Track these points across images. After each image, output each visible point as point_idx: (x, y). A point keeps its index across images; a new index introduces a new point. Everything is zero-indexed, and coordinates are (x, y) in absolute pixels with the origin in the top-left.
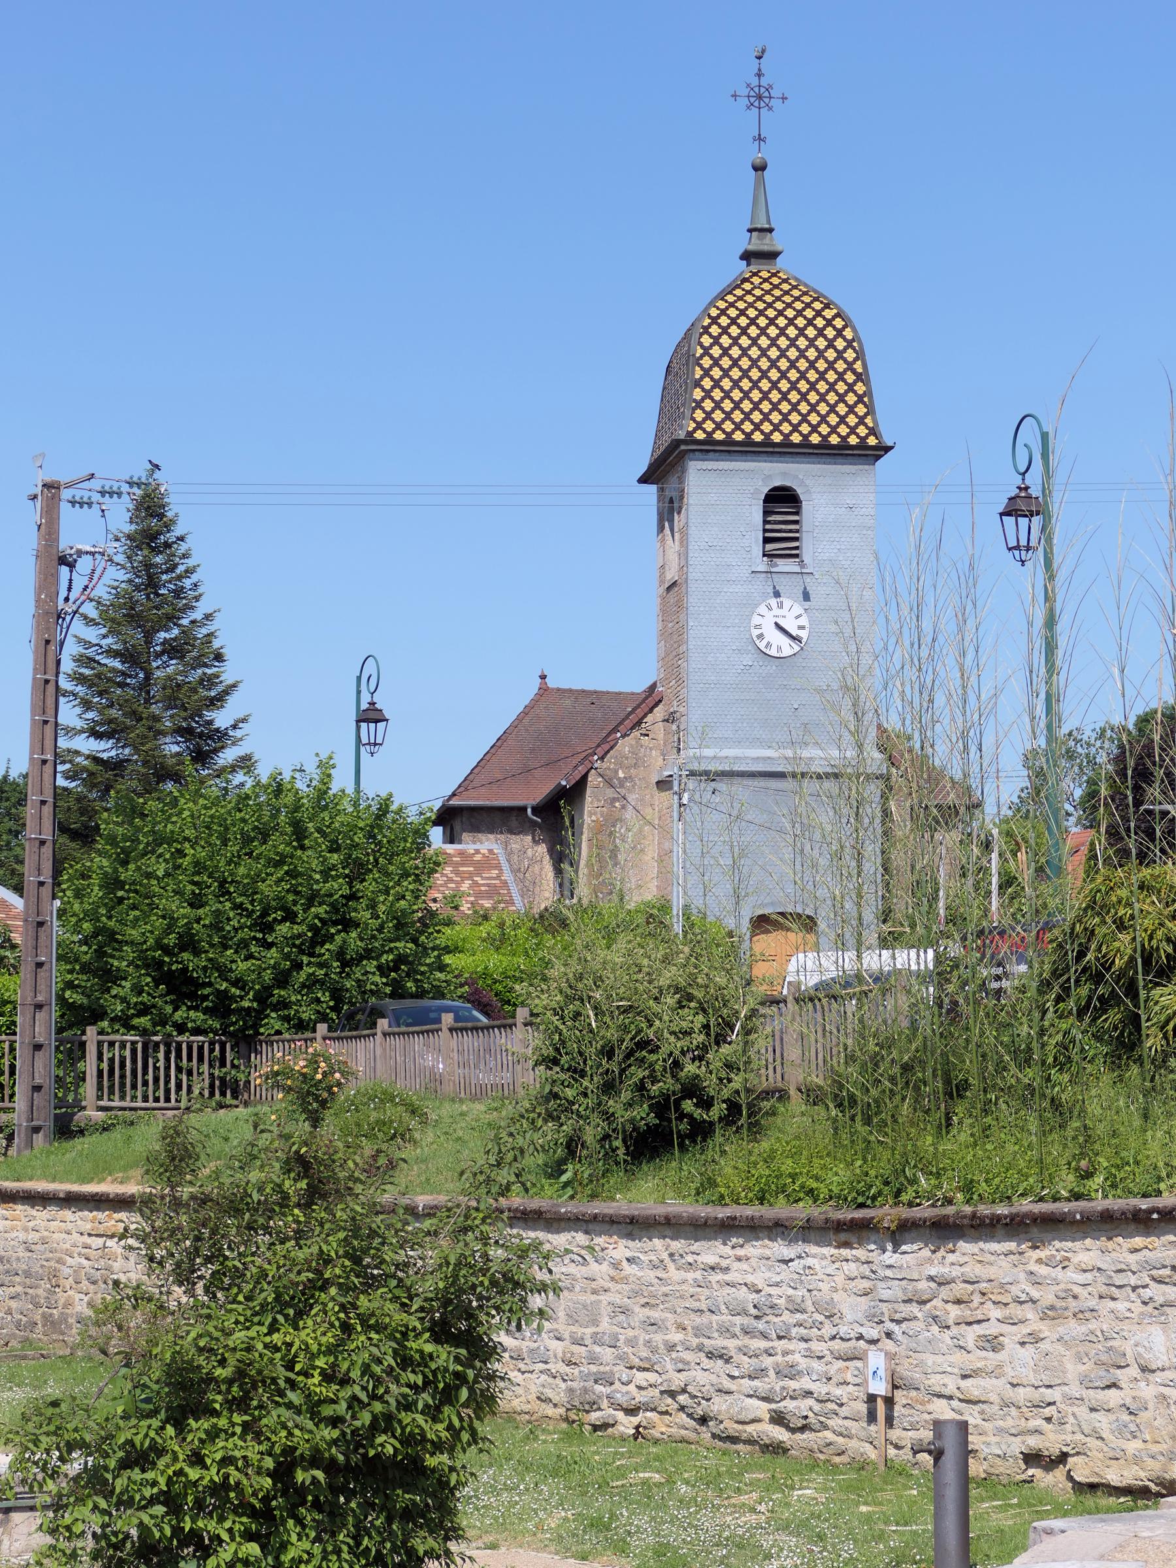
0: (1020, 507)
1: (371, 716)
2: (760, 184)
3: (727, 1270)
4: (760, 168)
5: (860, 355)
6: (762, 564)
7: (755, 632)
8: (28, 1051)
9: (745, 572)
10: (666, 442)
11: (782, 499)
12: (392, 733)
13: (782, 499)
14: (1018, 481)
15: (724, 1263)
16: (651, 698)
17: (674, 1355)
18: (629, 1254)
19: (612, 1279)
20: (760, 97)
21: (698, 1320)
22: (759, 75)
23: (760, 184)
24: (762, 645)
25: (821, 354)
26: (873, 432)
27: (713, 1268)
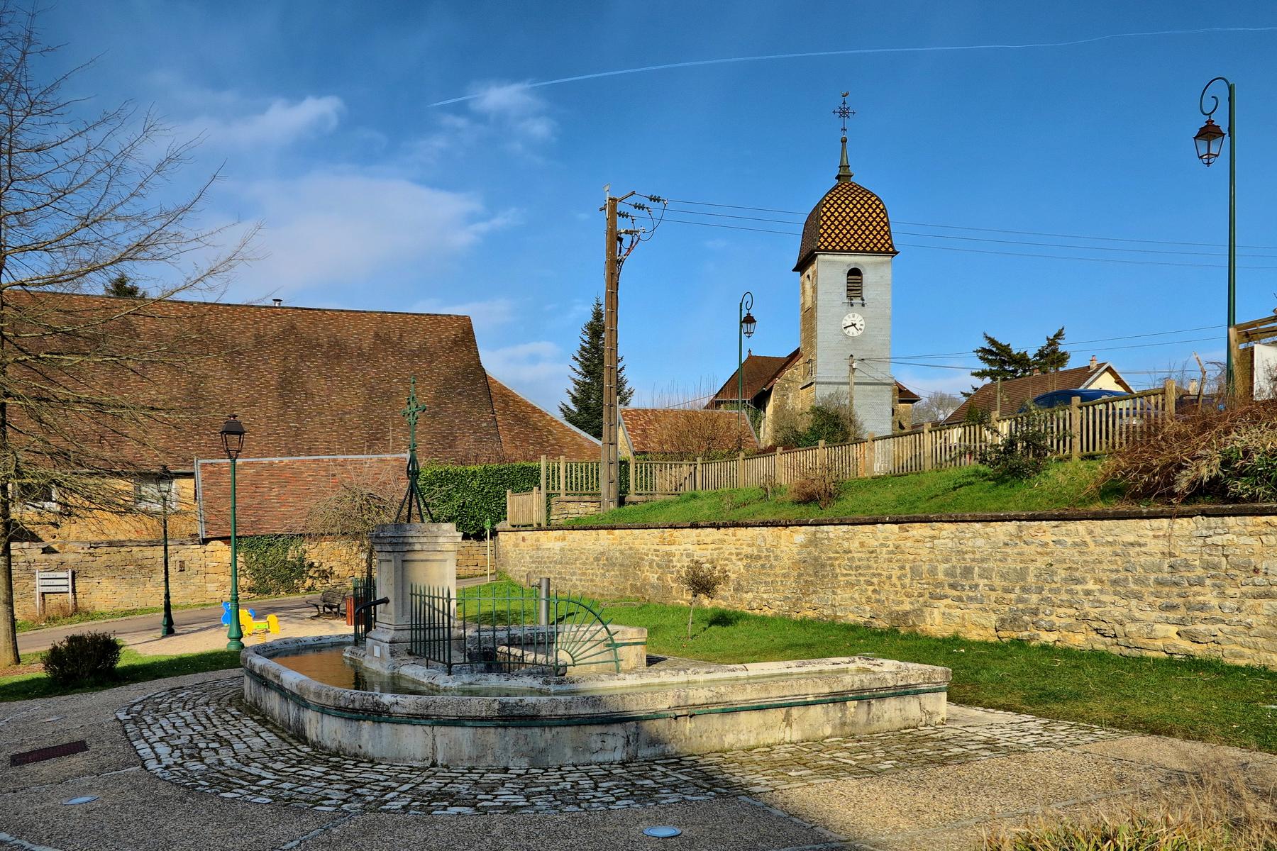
0: (1209, 132)
1: (749, 320)
2: (844, 147)
3: (1145, 545)
4: (844, 141)
5: (886, 215)
6: (846, 300)
8: (606, 465)
10: (806, 252)
11: (855, 272)
12: (758, 328)
13: (855, 272)
14: (1207, 118)
15: (1142, 541)
16: (795, 355)
17: (1091, 598)
18: (1054, 538)
19: (1039, 553)
20: (844, 113)
21: (1114, 576)
23: (844, 147)
25: (870, 215)
26: (891, 246)
27: (1132, 544)
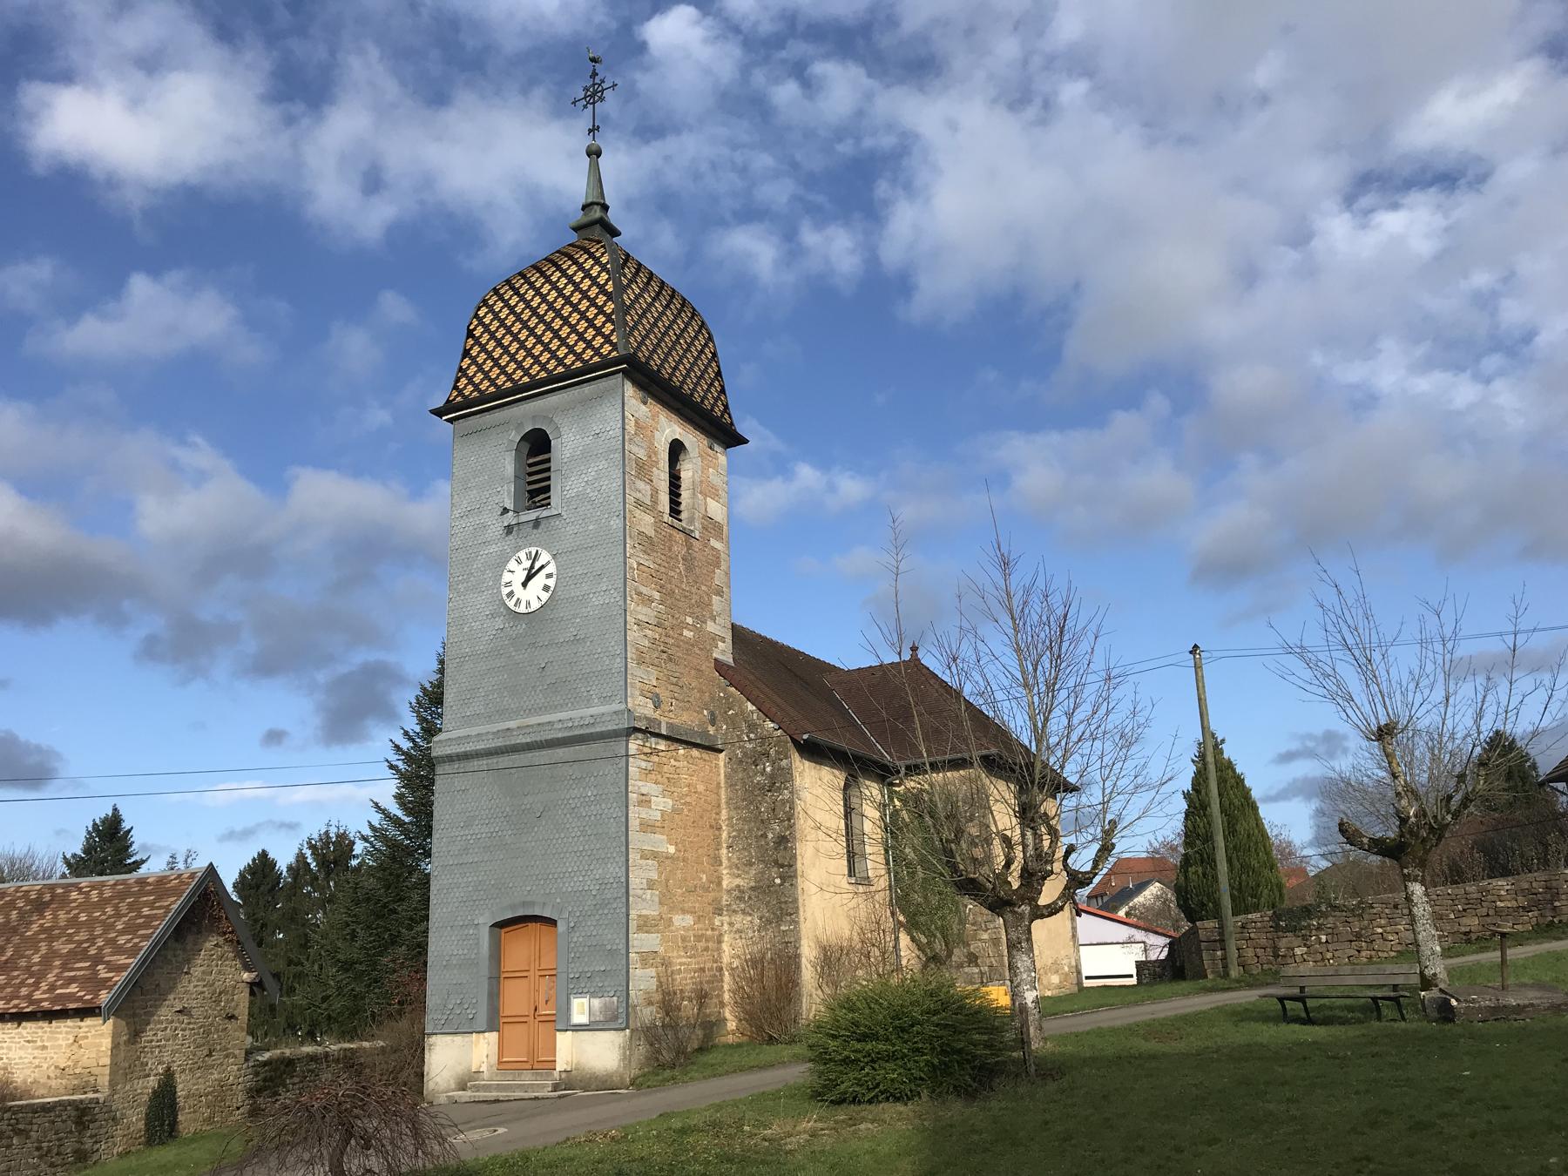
7: (505, 591)
9: (496, 526)
22: (594, 74)
23: (595, 171)
24: (511, 604)
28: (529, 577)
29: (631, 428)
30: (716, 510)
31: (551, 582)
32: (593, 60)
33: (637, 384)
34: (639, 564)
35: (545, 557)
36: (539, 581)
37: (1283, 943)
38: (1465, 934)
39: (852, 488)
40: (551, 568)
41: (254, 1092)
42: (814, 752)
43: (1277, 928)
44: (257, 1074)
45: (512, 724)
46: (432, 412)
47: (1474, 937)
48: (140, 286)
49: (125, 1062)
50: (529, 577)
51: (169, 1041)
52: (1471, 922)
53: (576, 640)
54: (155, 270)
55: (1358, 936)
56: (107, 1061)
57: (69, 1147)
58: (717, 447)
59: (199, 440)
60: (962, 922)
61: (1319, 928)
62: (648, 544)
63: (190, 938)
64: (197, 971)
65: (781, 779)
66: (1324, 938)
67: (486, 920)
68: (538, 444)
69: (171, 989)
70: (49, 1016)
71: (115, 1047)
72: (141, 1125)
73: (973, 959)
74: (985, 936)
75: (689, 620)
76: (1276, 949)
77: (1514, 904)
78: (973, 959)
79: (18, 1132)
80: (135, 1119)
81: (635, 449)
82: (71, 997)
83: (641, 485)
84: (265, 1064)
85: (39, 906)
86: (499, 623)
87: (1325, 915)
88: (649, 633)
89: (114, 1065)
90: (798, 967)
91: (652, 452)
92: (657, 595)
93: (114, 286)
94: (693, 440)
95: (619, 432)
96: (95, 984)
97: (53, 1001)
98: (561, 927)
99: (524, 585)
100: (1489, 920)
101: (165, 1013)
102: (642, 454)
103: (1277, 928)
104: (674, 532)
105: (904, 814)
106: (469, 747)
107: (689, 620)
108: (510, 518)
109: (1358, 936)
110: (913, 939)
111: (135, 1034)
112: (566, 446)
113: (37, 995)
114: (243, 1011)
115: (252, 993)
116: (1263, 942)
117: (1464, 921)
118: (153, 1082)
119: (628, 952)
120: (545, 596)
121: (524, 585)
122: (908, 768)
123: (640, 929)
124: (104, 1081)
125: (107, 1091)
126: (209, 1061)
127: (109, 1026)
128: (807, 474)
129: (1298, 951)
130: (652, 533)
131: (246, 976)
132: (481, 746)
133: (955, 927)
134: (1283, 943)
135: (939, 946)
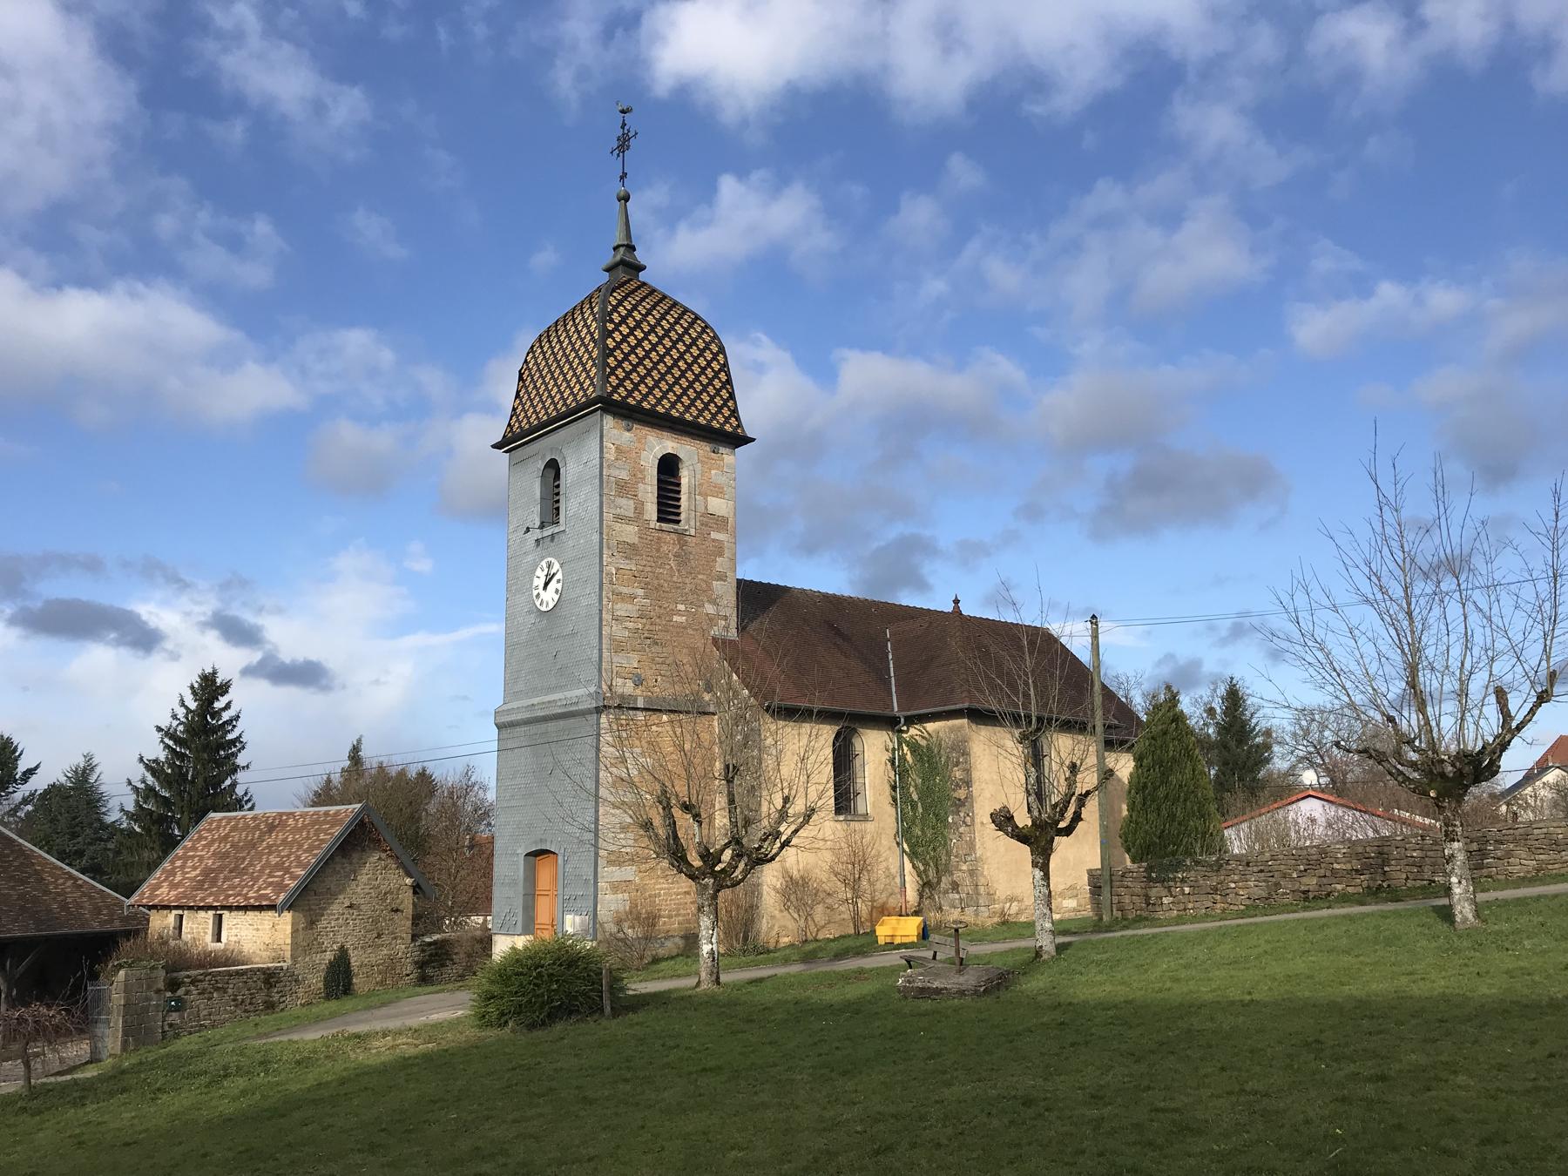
28: (546, 584)
29: (610, 455)
30: (717, 505)
31: (559, 586)
32: (623, 112)
33: (615, 415)
34: (618, 569)
35: (556, 566)
36: (553, 585)
37: (1154, 893)
38: (1304, 892)
39: (1444, 300)
40: (559, 576)
41: (421, 965)
42: (790, 713)
43: (1150, 879)
44: (423, 951)
45: (535, 701)
46: (494, 446)
47: (1311, 895)
48: (728, 186)
49: (304, 942)
50: (546, 584)
51: (341, 927)
52: (1311, 882)
53: (573, 634)
54: (742, 173)
55: (1215, 890)
56: (289, 941)
57: (260, 999)
58: (722, 450)
59: (764, 338)
60: (948, 854)
61: (1183, 880)
62: (629, 550)
63: (355, 856)
64: (363, 878)
65: (751, 739)
66: (1187, 890)
67: (522, 851)
68: (553, 468)
69: (342, 891)
70: (260, 908)
71: (295, 932)
72: (321, 985)
73: (955, 886)
74: (964, 867)
75: (681, 607)
76: (1147, 897)
77: (1349, 867)
78: (955, 886)
79: (217, 989)
80: (316, 981)
81: (615, 472)
82: (265, 897)
83: (623, 502)
84: (430, 944)
85: (271, 828)
86: (532, 619)
87: (1189, 869)
88: (631, 625)
89: (295, 945)
90: (760, 895)
91: (637, 473)
92: (640, 592)
93: (708, 193)
94: (687, 450)
95: (597, 461)
96: (280, 887)
97: (256, 899)
98: (560, 859)
99: (545, 588)
100: (1325, 880)
101: (336, 908)
102: (624, 475)
103: (1150, 879)
104: (664, 535)
105: (909, 757)
106: (513, 718)
107: (681, 607)
108: (537, 534)
109: (1215, 890)
110: (914, 867)
111: (312, 923)
112: (569, 473)
113: (251, 894)
114: (408, 910)
115: (415, 893)
116: (1138, 890)
117: (1304, 880)
118: (329, 956)
119: (596, 883)
120: (556, 597)
121: (545, 588)
122: (907, 718)
123: (610, 863)
124: (288, 954)
125: (289, 962)
126: (379, 942)
127: (288, 916)
128: (1389, 293)
129: (1165, 901)
130: (636, 540)
131: (408, 881)
132: (519, 717)
133: (944, 858)
134: (1154, 893)
135: (932, 873)
